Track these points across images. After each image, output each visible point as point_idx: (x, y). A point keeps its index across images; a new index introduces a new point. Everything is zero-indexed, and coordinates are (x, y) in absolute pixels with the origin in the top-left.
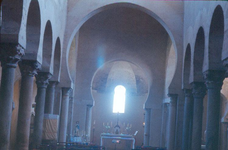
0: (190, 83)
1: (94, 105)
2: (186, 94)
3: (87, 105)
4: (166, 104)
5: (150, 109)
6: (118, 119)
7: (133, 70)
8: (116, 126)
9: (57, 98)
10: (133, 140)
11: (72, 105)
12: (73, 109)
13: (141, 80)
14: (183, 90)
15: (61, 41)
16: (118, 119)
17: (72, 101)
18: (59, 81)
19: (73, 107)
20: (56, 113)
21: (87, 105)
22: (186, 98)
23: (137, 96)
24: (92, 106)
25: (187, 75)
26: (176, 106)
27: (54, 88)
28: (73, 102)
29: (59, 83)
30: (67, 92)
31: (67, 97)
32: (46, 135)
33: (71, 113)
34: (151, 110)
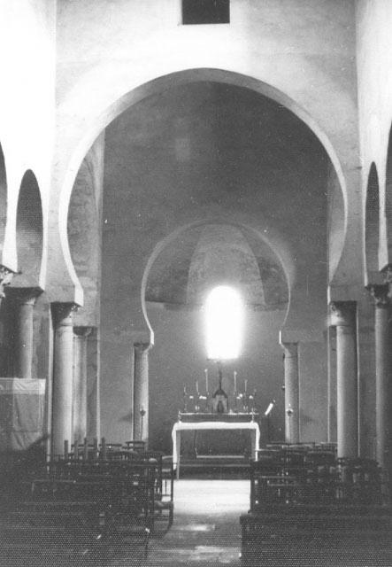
0: (380, 269)
1: (152, 342)
2: (377, 301)
3: (135, 345)
4: (334, 328)
5: (296, 344)
6: (220, 373)
7: (250, 245)
8: (217, 393)
9: (42, 332)
10: (254, 431)
11: (95, 348)
12: (99, 357)
13: (273, 269)
14: (369, 288)
15: (379, 174)
16: (220, 373)
17: (96, 335)
18: (43, 287)
19: (99, 352)
20: (40, 372)
21: (136, 345)
22: (378, 312)
23: (266, 310)
24: (147, 344)
25: (373, 246)
26: (355, 333)
27: (30, 306)
28: (99, 338)
29: (42, 291)
30: (65, 315)
31: (67, 328)
32: (14, 438)
33: (95, 367)
34: (299, 347)
